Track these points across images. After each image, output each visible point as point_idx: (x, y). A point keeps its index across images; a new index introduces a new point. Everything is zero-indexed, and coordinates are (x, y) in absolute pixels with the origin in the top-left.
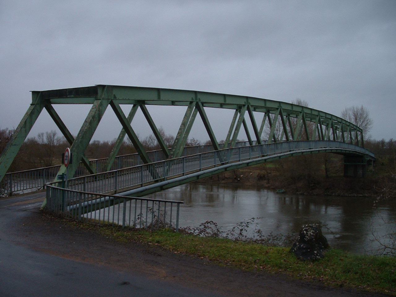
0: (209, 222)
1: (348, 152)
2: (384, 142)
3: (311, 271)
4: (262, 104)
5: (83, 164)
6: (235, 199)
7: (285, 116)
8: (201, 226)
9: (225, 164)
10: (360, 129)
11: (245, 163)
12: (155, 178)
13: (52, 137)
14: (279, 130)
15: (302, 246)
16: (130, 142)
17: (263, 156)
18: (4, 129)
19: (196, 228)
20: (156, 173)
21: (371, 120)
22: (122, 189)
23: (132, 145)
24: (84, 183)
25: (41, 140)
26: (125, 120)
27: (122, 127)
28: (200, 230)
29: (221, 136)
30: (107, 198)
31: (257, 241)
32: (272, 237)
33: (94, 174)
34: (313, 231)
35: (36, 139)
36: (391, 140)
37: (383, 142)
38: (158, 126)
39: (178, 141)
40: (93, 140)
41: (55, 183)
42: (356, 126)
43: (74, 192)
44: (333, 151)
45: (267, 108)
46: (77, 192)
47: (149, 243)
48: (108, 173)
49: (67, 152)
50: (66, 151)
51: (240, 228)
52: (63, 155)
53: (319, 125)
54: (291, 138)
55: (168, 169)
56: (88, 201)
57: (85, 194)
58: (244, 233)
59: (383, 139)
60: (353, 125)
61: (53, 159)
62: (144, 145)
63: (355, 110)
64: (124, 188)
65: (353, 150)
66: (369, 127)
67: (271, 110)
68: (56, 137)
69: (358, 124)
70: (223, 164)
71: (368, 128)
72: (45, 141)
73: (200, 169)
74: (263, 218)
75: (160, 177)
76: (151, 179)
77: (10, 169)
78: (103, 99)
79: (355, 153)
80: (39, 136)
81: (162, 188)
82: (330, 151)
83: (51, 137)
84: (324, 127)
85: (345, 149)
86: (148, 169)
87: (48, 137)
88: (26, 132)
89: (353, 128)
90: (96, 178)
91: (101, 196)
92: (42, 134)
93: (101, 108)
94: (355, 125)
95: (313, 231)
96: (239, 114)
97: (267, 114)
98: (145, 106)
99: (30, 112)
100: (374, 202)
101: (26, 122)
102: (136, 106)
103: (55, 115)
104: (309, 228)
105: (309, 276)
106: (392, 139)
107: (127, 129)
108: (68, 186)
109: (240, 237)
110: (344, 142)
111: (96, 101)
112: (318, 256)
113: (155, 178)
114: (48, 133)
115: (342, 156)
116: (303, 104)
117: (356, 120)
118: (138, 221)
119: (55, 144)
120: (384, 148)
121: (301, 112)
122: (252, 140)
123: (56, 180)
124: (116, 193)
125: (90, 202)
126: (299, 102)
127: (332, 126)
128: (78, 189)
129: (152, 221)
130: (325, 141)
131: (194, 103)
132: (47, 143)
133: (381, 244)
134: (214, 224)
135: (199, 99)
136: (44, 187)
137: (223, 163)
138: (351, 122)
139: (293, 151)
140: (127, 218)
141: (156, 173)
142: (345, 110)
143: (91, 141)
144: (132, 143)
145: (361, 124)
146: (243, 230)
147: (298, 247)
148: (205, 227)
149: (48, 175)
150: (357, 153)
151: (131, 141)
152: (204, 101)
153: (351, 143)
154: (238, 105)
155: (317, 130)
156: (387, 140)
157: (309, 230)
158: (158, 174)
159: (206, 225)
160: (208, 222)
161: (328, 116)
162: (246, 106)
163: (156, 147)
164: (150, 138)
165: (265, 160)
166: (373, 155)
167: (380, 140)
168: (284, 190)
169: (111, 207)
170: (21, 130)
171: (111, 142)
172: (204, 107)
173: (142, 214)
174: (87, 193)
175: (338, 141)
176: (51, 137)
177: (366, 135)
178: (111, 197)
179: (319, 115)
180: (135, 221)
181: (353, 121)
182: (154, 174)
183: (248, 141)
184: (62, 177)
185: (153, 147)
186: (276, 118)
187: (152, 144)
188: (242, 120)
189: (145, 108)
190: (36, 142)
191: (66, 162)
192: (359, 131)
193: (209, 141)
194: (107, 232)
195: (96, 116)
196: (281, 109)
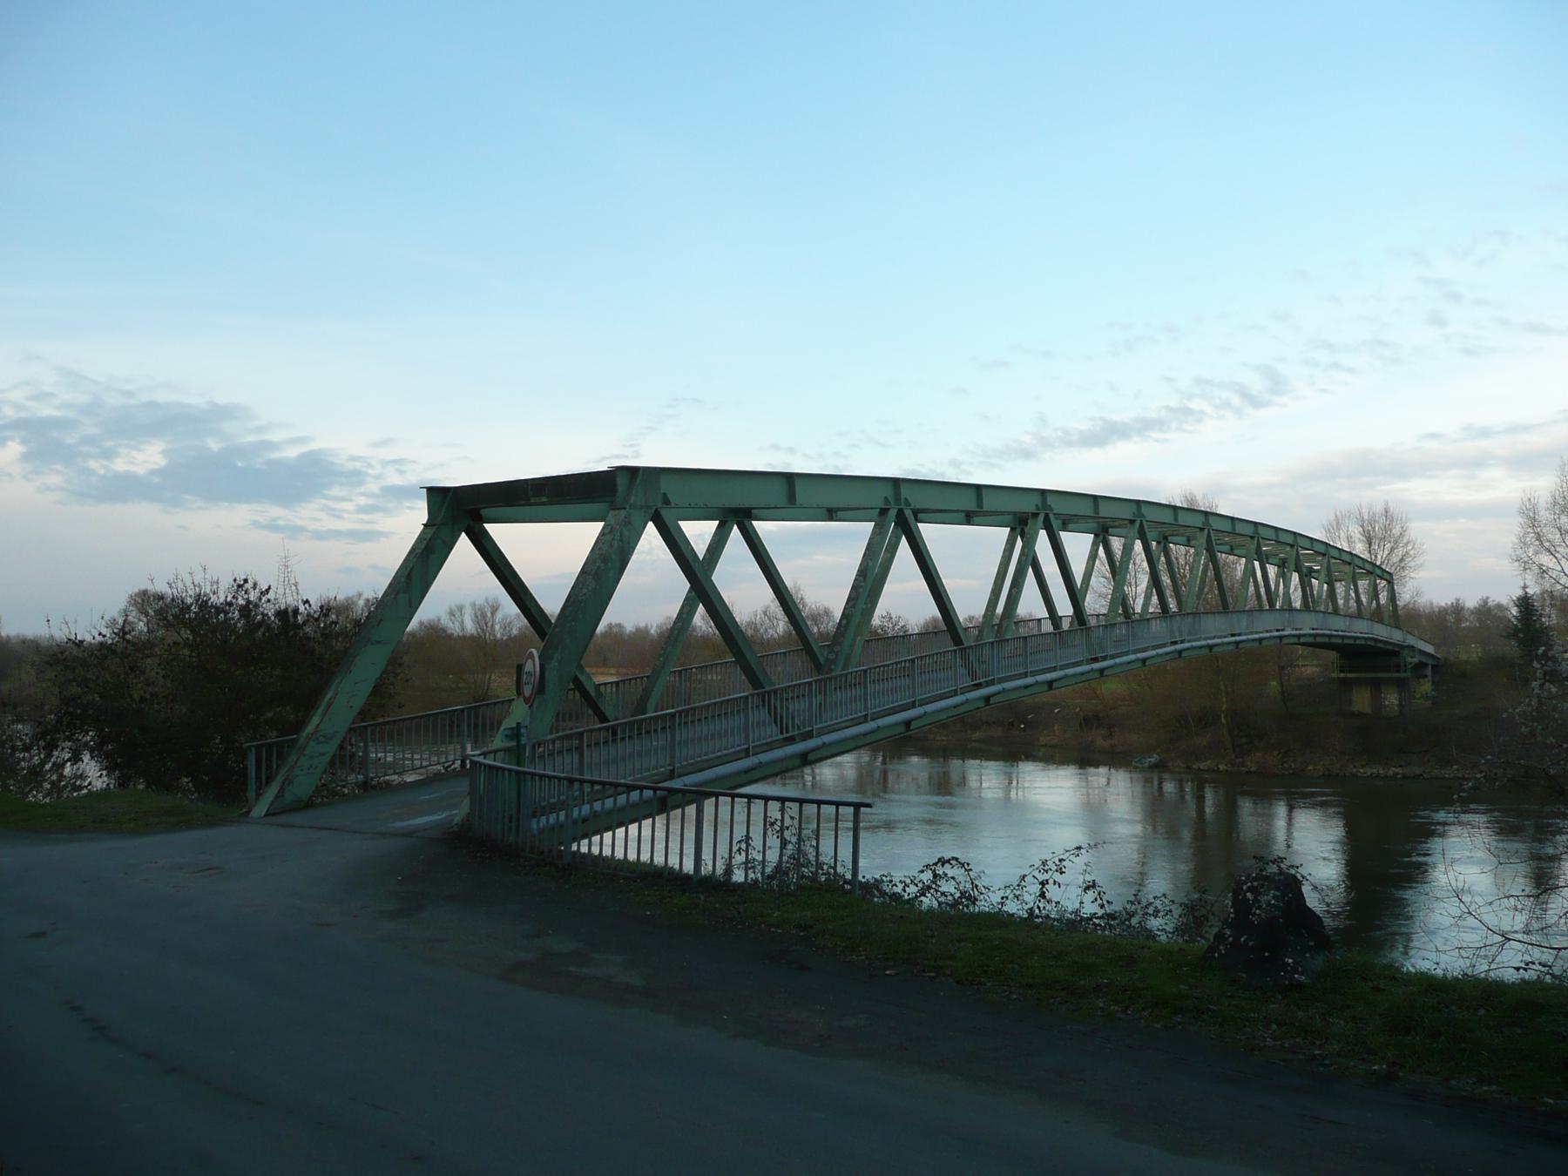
0: (948, 861)
1: (1351, 642)
2: (1463, 608)
3: (1280, 1024)
4: (1087, 509)
5: (576, 692)
6: (1015, 783)
7: (1154, 543)
8: (922, 871)
9: (984, 684)
10: (1385, 571)
11: (1043, 683)
12: (784, 731)
13: (489, 615)
14: (1136, 582)
15: (1242, 939)
16: (711, 627)
17: (1096, 660)
18: (350, 595)
19: (908, 881)
20: (787, 718)
21: (1418, 543)
22: (692, 764)
23: (715, 634)
24: (580, 749)
25: (457, 624)
26: (695, 566)
27: (689, 585)
28: (920, 885)
29: (970, 604)
30: (648, 793)
31: (1096, 918)
32: (1139, 907)
33: (609, 721)
34: (1277, 893)
35: (442, 622)
36: (1485, 602)
37: (1457, 610)
38: (788, 579)
39: (848, 623)
40: (606, 624)
41: (495, 752)
42: (1371, 563)
43: (550, 778)
44: (1302, 640)
45: (1101, 520)
46: (559, 779)
47: (773, 929)
48: (650, 718)
49: (530, 661)
50: (528, 658)
51: (1042, 877)
52: (520, 668)
53: (1257, 564)
54: (1173, 605)
55: (820, 704)
56: (591, 802)
57: (582, 782)
58: (1053, 892)
59: (1458, 600)
60: (1363, 559)
61: (493, 677)
62: (750, 632)
63: (1366, 517)
64: (697, 762)
65: (1366, 636)
66: (1412, 564)
67: (1112, 527)
68: (499, 616)
69: (1376, 557)
70: (979, 686)
71: (1410, 567)
72: (470, 627)
73: (914, 702)
74: (1105, 843)
75: (799, 728)
76: (772, 733)
77: (363, 714)
78: (631, 507)
79: (1372, 643)
80: (452, 613)
81: (806, 760)
82: (1296, 640)
83: (484, 614)
84: (1272, 571)
85: (1340, 633)
86: (763, 705)
87: (477, 617)
88: (410, 606)
89: (1361, 568)
90: (614, 733)
91: (630, 788)
92: (461, 608)
93: (626, 533)
94: (1368, 562)
95: (1277, 893)
96: (1019, 543)
97: (1101, 537)
98: (752, 524)
99: (423, 547)
100: (1455, 797)
101: (410, 574)
102: (727, 524)
103: (494, 556)
104: (1261, 882)
105: (1275, 1039)
106: (1488, 598)
107: (702, 589)
108: (532, 760)
109: (1041, 905)
110: (1336, 611)
111: (611, 512)
112: (1297, 972)
113: (784, 731)
114: (477, 603)
115: (1333, 655)
116: (1201, 504)
117: (1370, 545)
118: (739, 859)
119: (499, 635)
120: (1463, 625)
121: (1202, 529)
122: (1060, 615)
123: (498, 742)
124: (672, 775)
125: (597, 806)
126: (1192, 500)
127: (1296, 567)
128: (561, 767)
129: (781, 856)
130: (1277, 610)
131: (893, 513)
132: (475, 634)
133: (1488, 928)
134: (963, 866)
135: (906, 499)
136: (463, 762)
137: (978, 681)
138: (1354, 552)
139: (1182, 642)
140: (707, 855)
141: (787, 718)
142: (1332, 517)
143: (601, 623)
144: (717, 628)
145: (1384, 556)
146: (1048, 883)
147: (1231, 943)
148: (935, 875)
149: (476, 726)
150: (1380, 645)
151: (713, 624)
152: (919, 506)
153: (1359, 615)
154: (1015, 514)
155: (1252, 584)
156: (1471, 602)
157: (1262, 890)
158: (793, 719)
159: (940, 871)
160: (943, 862)
161: (1283, 538)
162: (1041, 517)
163: (785, 639)
164: (765, 613)
165: (1102, 671)
166: (1430, 649)
167: (1449, 603)
168: (1155, 755)
169: (660, 820)
170: (395, 598)
171: (657, 626)
172: (919, 524)
173: (751, 838)
174: (588, 781)
175: (1318, 609)
176: (484, 616)
177: (1405, 590)
178: (658, 792)
179: (1258, 534)
180: (731, 857)
181: (1360, 549)
182: (781, 717)
183: (1048, 616)
184: (515, 733)
185: (775, 639)
186: (1128, 550)
187: (770, 631)
188: (1031, 558)
189: (750, 529)
190: (444, 630)
191: (527, 691)
192: (1382, 578)
193: (935, 620)
194: (649, 895)
195: (613, 557)
196: (1141, 522)
